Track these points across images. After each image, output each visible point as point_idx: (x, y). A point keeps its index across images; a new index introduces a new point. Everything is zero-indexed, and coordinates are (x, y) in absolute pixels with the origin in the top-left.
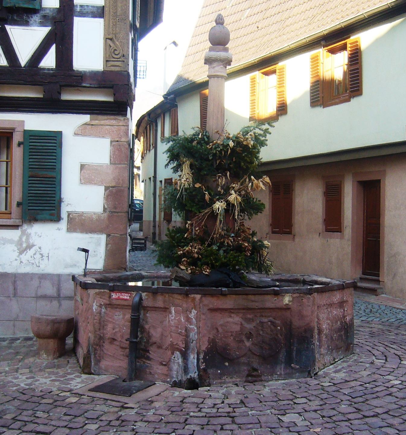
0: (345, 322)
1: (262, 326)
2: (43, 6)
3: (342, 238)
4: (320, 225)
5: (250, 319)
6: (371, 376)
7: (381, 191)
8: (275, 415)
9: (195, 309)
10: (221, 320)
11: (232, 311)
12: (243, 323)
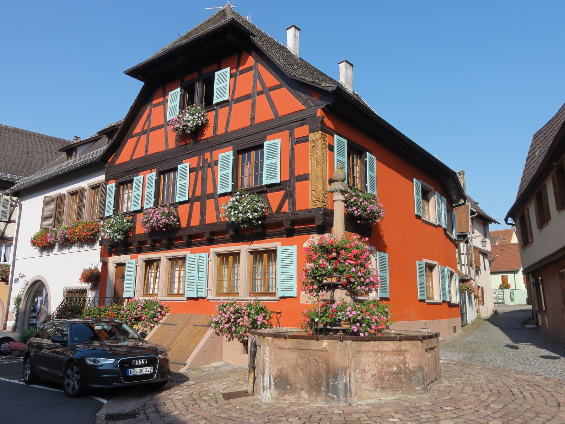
1: (309, 362)
2: (174, 147)
7: (143, 63)
11: (291, 350)
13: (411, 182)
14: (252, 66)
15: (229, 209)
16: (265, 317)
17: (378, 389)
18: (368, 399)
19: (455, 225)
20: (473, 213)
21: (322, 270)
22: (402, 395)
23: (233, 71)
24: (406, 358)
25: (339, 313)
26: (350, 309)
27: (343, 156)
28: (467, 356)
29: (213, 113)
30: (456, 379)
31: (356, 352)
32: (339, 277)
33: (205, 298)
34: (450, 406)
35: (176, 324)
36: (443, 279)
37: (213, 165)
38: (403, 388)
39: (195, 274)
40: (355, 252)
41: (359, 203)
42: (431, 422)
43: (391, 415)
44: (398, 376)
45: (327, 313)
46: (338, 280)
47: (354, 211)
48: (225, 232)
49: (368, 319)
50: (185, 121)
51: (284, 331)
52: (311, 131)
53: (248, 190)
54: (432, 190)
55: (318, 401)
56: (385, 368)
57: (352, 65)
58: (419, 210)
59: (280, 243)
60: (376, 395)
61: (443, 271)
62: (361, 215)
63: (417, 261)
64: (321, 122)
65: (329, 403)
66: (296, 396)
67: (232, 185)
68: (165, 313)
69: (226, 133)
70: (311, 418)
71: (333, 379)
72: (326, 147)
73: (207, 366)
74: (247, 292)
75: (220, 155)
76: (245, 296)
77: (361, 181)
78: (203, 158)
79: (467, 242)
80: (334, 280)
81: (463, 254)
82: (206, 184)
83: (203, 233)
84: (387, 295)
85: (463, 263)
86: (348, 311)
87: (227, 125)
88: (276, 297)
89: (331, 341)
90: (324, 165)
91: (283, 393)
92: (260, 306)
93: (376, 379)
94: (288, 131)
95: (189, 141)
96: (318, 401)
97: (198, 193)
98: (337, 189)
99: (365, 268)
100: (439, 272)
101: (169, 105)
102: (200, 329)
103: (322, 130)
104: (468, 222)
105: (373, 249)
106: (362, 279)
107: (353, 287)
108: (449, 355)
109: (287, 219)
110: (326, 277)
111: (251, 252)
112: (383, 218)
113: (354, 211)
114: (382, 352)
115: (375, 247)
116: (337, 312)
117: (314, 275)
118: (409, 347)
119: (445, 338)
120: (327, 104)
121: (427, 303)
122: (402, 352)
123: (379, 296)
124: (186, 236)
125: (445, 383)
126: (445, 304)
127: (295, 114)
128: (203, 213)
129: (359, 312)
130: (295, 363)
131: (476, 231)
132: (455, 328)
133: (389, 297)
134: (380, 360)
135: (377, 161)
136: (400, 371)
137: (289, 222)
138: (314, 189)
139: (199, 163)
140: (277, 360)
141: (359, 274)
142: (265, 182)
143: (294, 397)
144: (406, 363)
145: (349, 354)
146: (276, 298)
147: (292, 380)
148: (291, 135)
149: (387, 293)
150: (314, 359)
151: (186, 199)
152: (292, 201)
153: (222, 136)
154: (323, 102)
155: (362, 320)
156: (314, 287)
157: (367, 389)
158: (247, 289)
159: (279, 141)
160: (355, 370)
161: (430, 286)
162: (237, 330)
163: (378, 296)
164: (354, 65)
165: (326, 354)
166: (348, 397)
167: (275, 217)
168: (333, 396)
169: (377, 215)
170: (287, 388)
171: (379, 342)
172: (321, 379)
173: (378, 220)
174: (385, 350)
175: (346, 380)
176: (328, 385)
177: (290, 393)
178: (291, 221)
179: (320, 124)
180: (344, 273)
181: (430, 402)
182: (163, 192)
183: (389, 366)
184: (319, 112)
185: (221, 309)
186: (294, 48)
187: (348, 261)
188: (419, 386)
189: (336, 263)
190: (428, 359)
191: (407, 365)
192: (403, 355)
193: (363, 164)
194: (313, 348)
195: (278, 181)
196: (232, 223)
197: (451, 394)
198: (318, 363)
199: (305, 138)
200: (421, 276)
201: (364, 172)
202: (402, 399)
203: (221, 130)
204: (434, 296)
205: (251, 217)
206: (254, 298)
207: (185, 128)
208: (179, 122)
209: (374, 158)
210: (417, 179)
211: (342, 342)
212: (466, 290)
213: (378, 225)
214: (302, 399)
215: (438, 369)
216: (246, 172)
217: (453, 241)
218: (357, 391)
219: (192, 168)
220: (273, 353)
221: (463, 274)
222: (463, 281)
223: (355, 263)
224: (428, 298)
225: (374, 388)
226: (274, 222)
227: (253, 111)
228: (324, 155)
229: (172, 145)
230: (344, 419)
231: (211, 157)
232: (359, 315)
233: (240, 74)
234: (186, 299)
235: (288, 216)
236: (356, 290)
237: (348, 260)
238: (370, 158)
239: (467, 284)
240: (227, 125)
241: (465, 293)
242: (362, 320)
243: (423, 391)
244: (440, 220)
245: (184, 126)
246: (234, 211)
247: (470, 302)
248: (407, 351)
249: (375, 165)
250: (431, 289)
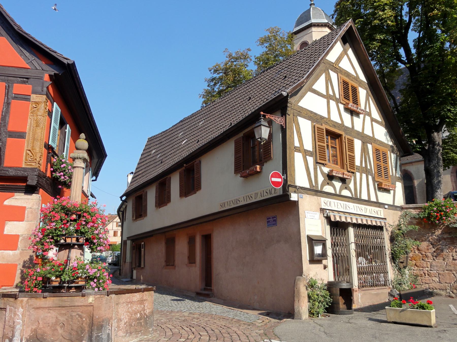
0: (145, 314)
1: (72, 319)
3: (196, 266)
4: (186, 260)
8: (307, 338)
9: (22, 308)
10: (42, 314)
12: (59, 316)
47: (60, 176)
52: (34, 92)
71: (97, 330)
80: (74, 240)
98: (81, 157)
113: (60, 176)
127: (16, 70)
130: (54, 321)
136: (141, 317)
140: (32, 320)
148: (8, 89)
150: (78, 315)
154: (53, 70)
175: (109, 330)
184: (46, 77)
193: (62, 135)
194: (77, 304)
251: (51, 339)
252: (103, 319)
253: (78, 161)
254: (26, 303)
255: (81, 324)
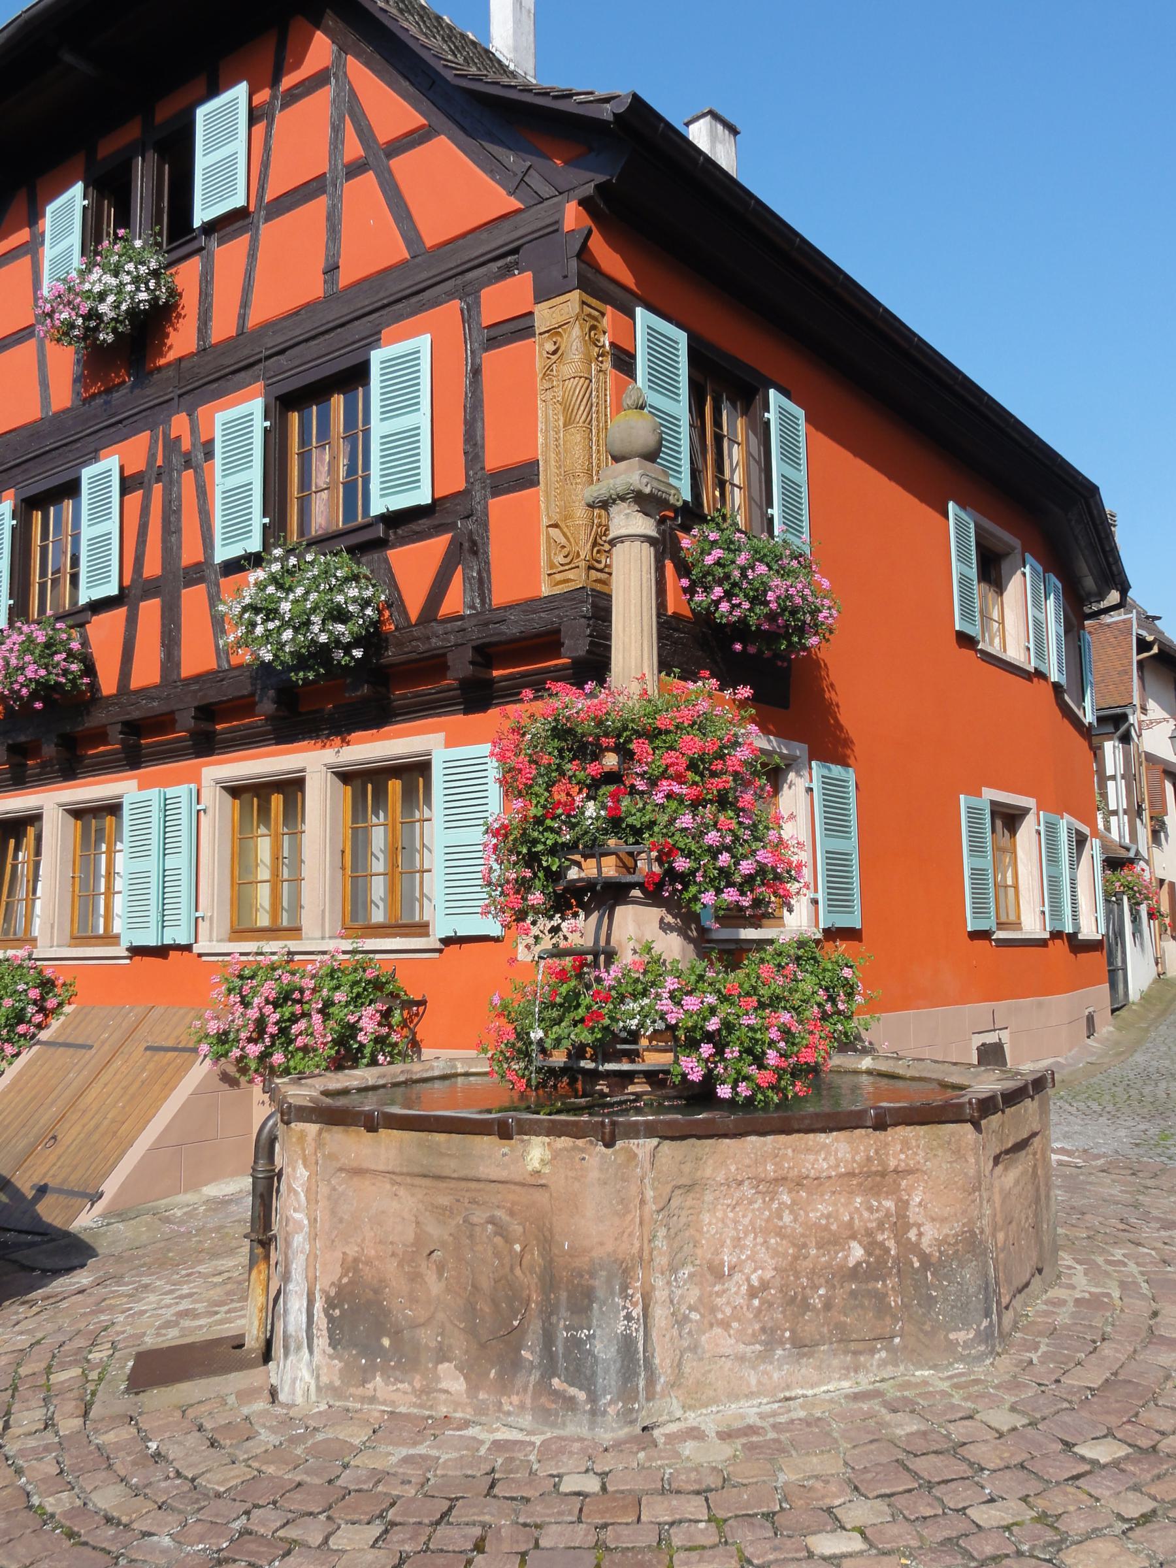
2: (69, 405)
5: (445, 1209)
6: (1011, 1533)
9: (305, 1166)
11: (399, 1179)
13: (938, 517)
14: (327, 69)
15: (246, 616)
16: (386, 1015)
17: (779, 1352)
18: (734, 1396)
19: (1090, 678)
20: (1143, 645)
21: (560, 828)
22: (890, 1368)
23: (258, 99)
24: (907, 1202)
25: (632, 1006)
26: (676, 986)
27: (674, 395)
28: (1145, 1131)
29: (195, 263)
30: (1118, 1254)
31: (679, 1187)
32: (631, 854)
33: (188, 948)
34: (1110, 1434)
35: (89, 1042)
36: (1053, 859)
37: (201, 456)
38: (892, 1338)
39: (151, 864)
40: (693, 744)
41: (736, 574)
42: (1019, 1554)
43: (828, 1502)
44: (870, 1286)
45: (578, 1006)
46: (625, 866)
47: (717, 603)
48: (242, 706)
49: (751, 1028)
50: (88, 295)
51: (436, 1073)
52: (542, 295)
53: (322, 542)
54: (1013, 549)
55: (509, 1414)
56: (813, 1252)
57: (733, 131)
58: (967, 614)
59: (441, 736)
60: (770, 1378)
61: (1052, 829)
62: (743, 620)
63: (962, 797)
64: (579, 255)
65: (553, 1425)
66: (417, 1385)
67: (264, 525)
68: (60, 1005)
69: (241, 333)
70: (442, 1530)
72: (602, 355)
73: (189, 1197)
74: (333, 923)
75: (221, 418)
76: (323, 938)
77: (749, 499)
78: (166, 435)
79: (1126, 739)
80: (610, 868)
81: (1113, 778)
82: (178, 531)
83: (172, 712)
84: (854, 920)
85: (1112, 806)
86: (666, 995)
87: (245, 304)
88: (432, 938)
89: (564, 1142)
90: (594, 423)
91: (364, 1370)
92: (369, 975)
93: (771, 1305)
94: (458, 301)
95: (118, 376)
96: (509, 1414)
97: (153, 568)
98: (621, 489)
99: (738, 811)
100: (1038, 832)
101: (49, 253)
102: (165, 1061)
103: (584, 285)
104: (1127, 672)
105: (798, 753)
106: (724, 859)
107: (687, 896)
108: (1077, 1128)
109: (460, 641)
110: (577, 857)
111: (346, 776)
112: (831, 632)
113: (717, 603)
114: (799, 1183)
115: (806, 746)
116: (622, 999)
117: (529, 849)
118: (920, 1157)
119: (1059, 1059)
120: (601, 178)
121: (997, 940)
122: (889, 1179)
123: (822, 926)
124: (119, 727)
125: (1074, 1280)
126: (1058, 942)
127: (484, 235)
128: (170, 640)
129: (711, 999)
130: (410, 1236)
131: (1152, 705)
132: (1090, 1019)
133: (858, 927)
134: (787, 1218)
135: (812, 430)
136: (881, 1262)
137: (469, 654)
138: (556, 518)
139: (152, 457)
140: (341, 1221)
141: (712, 837)
142: (377, 507)
143: (409, 1390)
144: (908, 1227)
145: (643, 1202)
146: (432, 942)
147: (403, 1311)
148: (469, 316)
149: (853, 913)
150: (492, 1221)
151: (112, 589)
152: (479, 572)
153: (229, 344)
154: (589, 175)
155: (724, 1033)
156: (530, 897)
157: (728, 1351)
158: (332, 912)
159: (423, 342)
160: (673, 1269)
161: (1009, 882)
162: (292, 1063)
163: (817, 925)
164: (739, 128)
165: (541, 1197)
166: (636, 1399)
167: (417, 639)
168: (573, 1391)
169: (808, 618)
170: (382, 1346)
171: (782, 1138)
172: (519, 1312)
173: (813, 641)
174: (812, 1174)
175: (628, 1317)
176: (548, 1338)
177: (393, 1368)
178: (478, 649)
179: (574, 263)
180: (646, 835)
181: (1013, 1409)
182: (43, 573)
183: (832, 1241)
184: (572, 216)
185: (234, 989)
186: (516, 49)
187: (665, 785)
188: (967, 1325)
189: (615, 797)
190: (1006, 1196)
191: (912, 1235)
192: (895, 1190)
193: (755, 434)
195: (423, 497)
196: (265, 667)
197: (1107, 1349)
198: (509, 1241)
199: (522, 324)
200: (977, 849)
201: (758, 463)
202: (892, 1393)
203: (223, 328)
204: (1023, 918)
205: (323, 638)
206: (347, 945)
207: (93, 324)
208: (69, 302)
209: (800, 413)
210: (962, 504)
211: (609, 1144)
212: (1123, 893)
213: (813, 666)
214: (443, 1397)
215: (1045, 1226)
216: (320, 477)
217: (1086, 732)
218: (679, 1364)
219: (132, 476)
220: (324, 1190)
221: (1112, 841)
222: (1114, 863)
223: (695, 791)
224: (1001, 925)
225: (758, 1347)
226: (414, 656)
227: (334, 241)
228: (594, 385)
229: (63, 396)
230: (591, 1540)
231: (194, 430)
232: (713, 1011)
233: (284, 106)
234: (126, 954)
235: (464, 630)
236: (698, 908)
237: (665, 783)
238: (782, 411)
239: (1125, 874)
240: (245, 304)
241: (1119, 903)
242: (724, 1033)
243: (982, 1348)
244: (1041, 654)
245: (87, 317)
246: (267, 620)
247: (1137, 931)
248: (909, 1172)
249: (802, 439)
250: (1011, 891)
251: (405, 1316)
252: (592, 1260)
253: (619, 512)
254: (313, 1144)
255: (508, 1269)
